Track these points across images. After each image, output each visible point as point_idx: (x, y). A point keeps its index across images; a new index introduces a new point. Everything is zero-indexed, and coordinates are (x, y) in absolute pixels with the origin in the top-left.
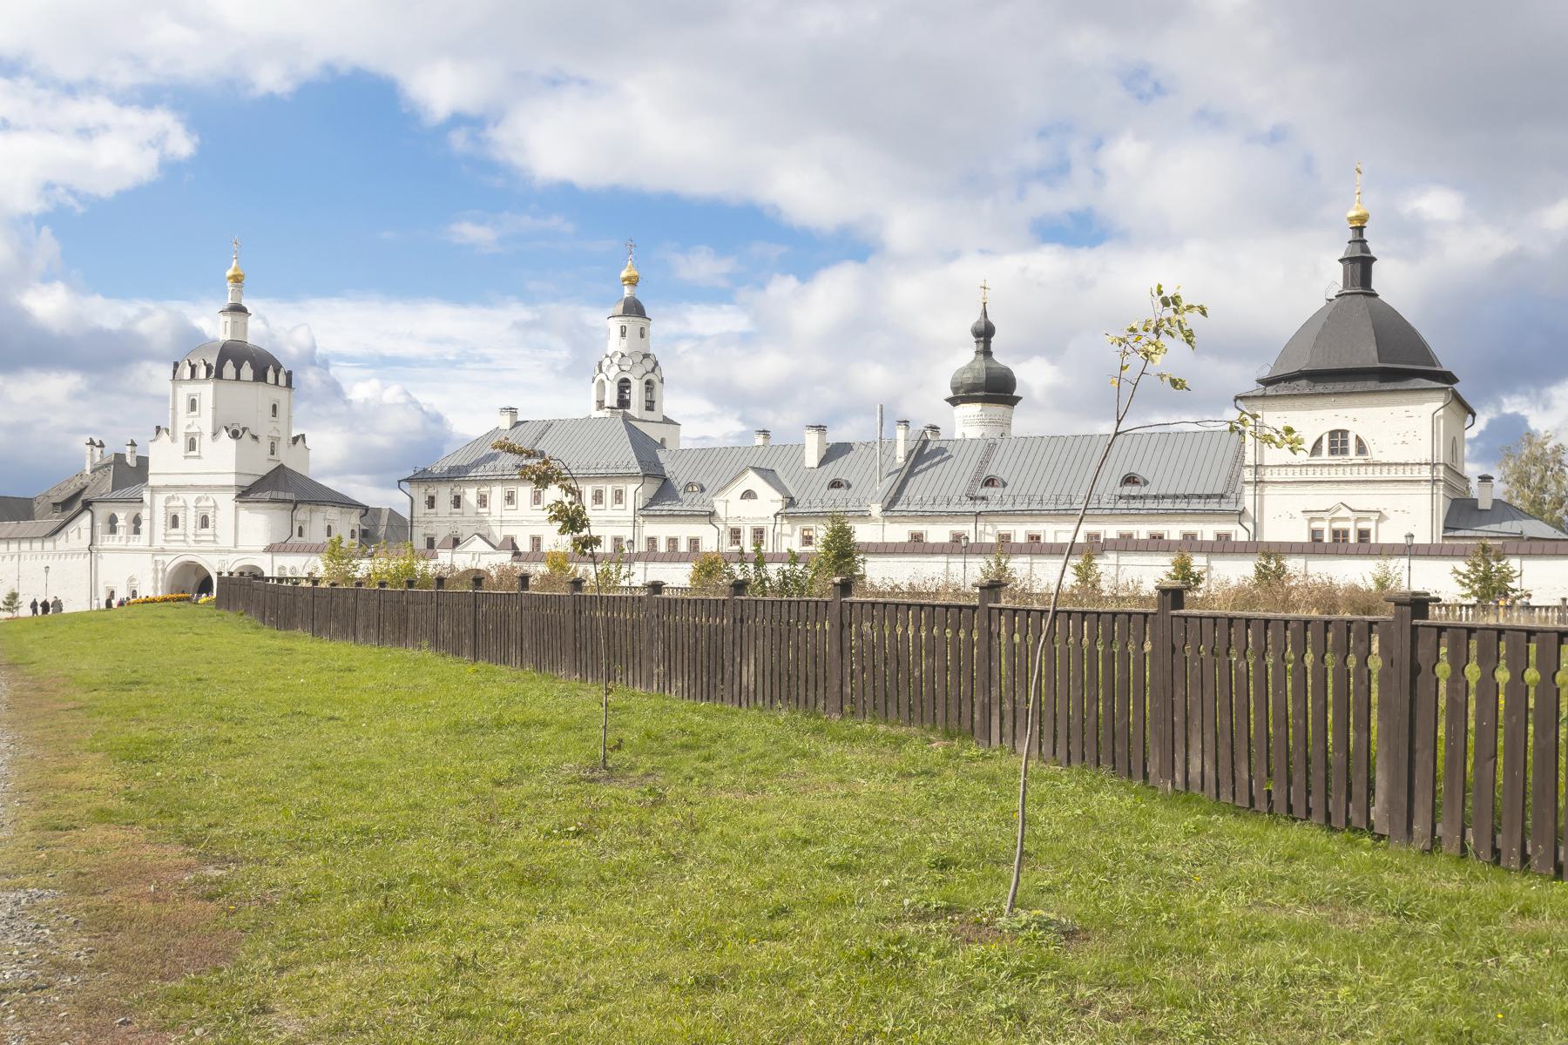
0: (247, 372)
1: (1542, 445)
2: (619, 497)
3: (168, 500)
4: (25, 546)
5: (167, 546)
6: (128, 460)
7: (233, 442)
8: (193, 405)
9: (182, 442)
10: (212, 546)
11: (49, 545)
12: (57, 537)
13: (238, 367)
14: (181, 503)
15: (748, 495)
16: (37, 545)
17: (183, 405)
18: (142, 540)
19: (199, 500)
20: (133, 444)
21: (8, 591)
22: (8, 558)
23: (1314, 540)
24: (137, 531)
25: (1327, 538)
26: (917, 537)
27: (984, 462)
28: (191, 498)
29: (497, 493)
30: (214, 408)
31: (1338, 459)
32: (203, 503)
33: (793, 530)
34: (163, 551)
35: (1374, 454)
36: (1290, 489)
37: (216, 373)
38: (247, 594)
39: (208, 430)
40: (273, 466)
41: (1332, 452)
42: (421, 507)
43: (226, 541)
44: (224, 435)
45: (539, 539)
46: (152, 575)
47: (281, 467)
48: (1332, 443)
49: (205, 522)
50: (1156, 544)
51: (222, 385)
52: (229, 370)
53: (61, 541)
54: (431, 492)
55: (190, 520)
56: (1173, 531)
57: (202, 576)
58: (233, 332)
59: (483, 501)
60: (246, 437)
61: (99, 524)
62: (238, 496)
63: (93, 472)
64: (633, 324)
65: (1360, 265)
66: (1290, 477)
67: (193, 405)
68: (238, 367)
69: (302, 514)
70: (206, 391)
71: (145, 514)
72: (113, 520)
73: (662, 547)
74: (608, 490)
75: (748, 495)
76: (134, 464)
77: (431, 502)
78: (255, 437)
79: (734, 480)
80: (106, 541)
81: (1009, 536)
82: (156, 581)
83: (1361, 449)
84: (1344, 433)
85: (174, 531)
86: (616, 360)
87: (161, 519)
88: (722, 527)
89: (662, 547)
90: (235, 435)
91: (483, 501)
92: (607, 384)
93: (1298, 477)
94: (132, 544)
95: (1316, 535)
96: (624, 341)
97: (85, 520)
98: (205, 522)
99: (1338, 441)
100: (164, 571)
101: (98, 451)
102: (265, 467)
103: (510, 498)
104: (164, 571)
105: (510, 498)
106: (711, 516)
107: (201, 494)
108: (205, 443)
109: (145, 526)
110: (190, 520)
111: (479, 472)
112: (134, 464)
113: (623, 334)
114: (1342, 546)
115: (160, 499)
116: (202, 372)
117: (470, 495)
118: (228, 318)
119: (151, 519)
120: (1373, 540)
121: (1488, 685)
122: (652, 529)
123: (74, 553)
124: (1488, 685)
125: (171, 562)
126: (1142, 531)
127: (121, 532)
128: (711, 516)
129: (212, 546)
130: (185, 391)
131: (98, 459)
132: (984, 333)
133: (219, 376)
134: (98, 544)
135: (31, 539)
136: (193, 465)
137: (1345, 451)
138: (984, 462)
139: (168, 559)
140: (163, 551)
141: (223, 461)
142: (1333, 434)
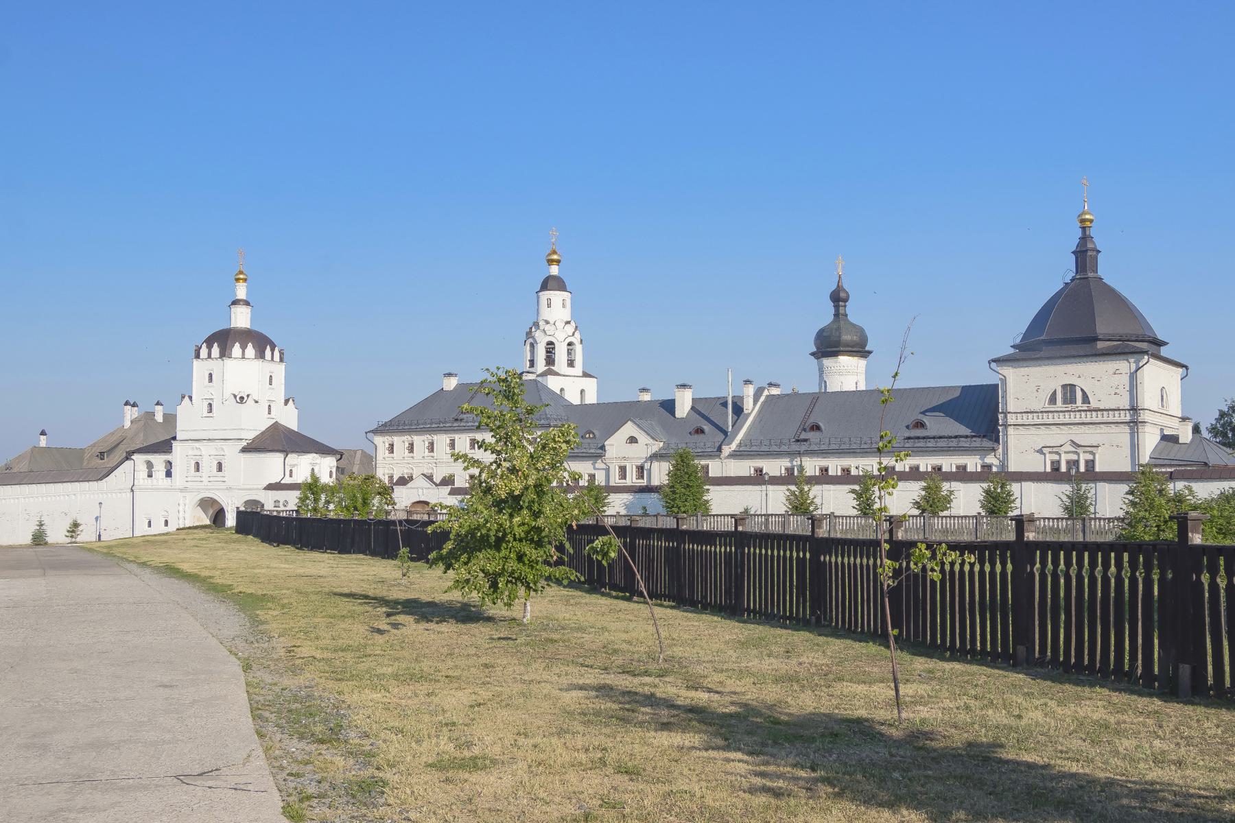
1: (385, 492)
15: (633, 440)
21: (71, 521)
25: (1063, 469)
26: (759, 471)
27: (810, 412)
31: (1070, 407)
35: (1094, 404)
36: (1033, 430)
38: (255, 523)
41: (1065, 402)
48: (1064, 395)
50: (914, 474)
56: (925, 463)
57: (216, 508)
60: (250, 402)
65: (1084, 255)
66: (1030, 421)
69: (293, 458)
72: (150, 465)
75: (633, 440)
83: (1086, 399)
84: (1073, 386)
93: (1037, 421)
95: (1056, 466)
99: (1069, 390)
110: (209, 466)
121: (760, 553)
124: (760, 553)
126: (903, 466)
132: (838, 298)
137: (1073, 401)
138: (810, 412)
142: (1064, 387)
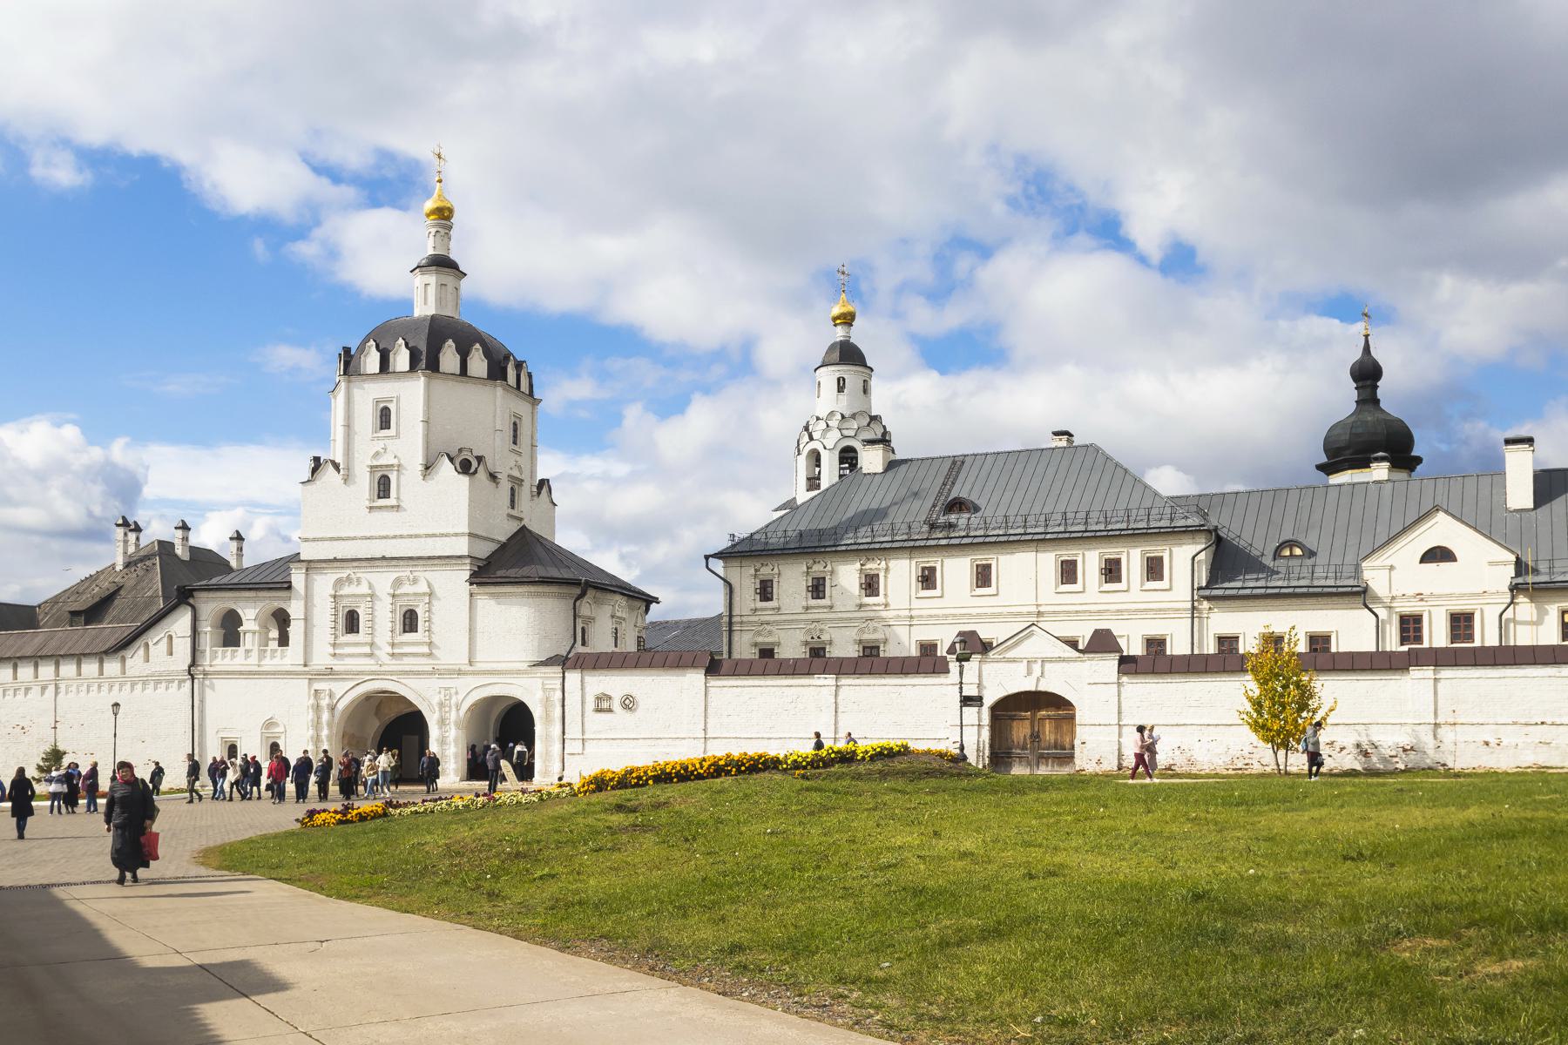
0: (478, 364)
2: (1154, 569)
3: (339, 583)
4: (68, 669)
5: (338, 666)
6: (179, 551)
7: (465, 479)
8: (385, 419)
9: (364, 482)
10: (424, 664)
11: (112, 667)
12: (128, 653)
13: (464, 354)
14: (364, 589)
15: (1438, 555)
16: (90, 668)
17: (366, 417)
18: (292, 655)
19: (398, 582)
20: (185, 527)
22: (36, 690)
23: (1313, 650)
24: (284, 640)
28: (382, 580)
29: (899, 573)
30: (426, 422)
32: (406, 588)
33: (1542, 614)
34: (330, 673)
37: (426, 361)
39: (418, 460)
40: (514, 527)
42: (747, 598)
43: (452, 651)
44: (446, 469)
45: (1469, 617)
46: (311, 715)
47: (523, 530)
49: (410, 621)
51: (440, 385)
52: (449, 358)
53: (135, 660)
54: (766, 571)
55: (381, 620)
58: (440, 301)
59: (870, 585)
60: (482, 475)
61: (206, 628)
62: (474, 575)
63: (127, 565)
64: (850, 373)
67: (385, 419)
68: (464, 354)
70: (410, 394)
71: (295, 609)
73: (1437, 635)
74: (1133, 559)
76: (186, 557)
77: (765, 591)
78: (493, 477)
79: (1405, 530)
80: (219, 659)
81: (1326, 639)
82: (317, 725)
85: (351, 638)
86: (834, 423)
87: (325, 617)
88: (1383, 613)
89: (1437, 635)
90: (465, 468)
91: (870, 585)
92: (825, 456)
94: (269, 664)
96: (843, 397)
97: (181, 623)
98: (410, 621)
100: (332, 708)
101: (132, 536)
102: (503, 530)
103: (927, 579)
104: (332, 708)
105: (927, 579)
106: (1360, 595)
107: (404, 572)
108: (408, 484)
109: (295, 630)
110: (381, 620)
111: (864, 536)
112: (186, 557)
113: (841, 389)
114: (1321, 657)
115: (324, 584)
116: (401, 360)
117: (847, 576)
118: (432, 279)
119: (307, 620)
120: (1333, 650)
122: (1223, 621)
123: (158, 680)
125: (346, 694)
127: (248, 641)
128: (1360, 595)
129: (424, 664)
130: (368, 395)
131: (131, 549)
133: (433, 366)
134: (206, 662)
135: (79, 657)
136: (385, 522)
139: (339, 688)
140: (330, 673)
141: (445, 511)
